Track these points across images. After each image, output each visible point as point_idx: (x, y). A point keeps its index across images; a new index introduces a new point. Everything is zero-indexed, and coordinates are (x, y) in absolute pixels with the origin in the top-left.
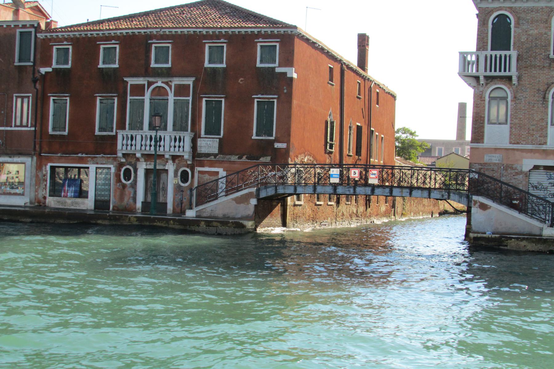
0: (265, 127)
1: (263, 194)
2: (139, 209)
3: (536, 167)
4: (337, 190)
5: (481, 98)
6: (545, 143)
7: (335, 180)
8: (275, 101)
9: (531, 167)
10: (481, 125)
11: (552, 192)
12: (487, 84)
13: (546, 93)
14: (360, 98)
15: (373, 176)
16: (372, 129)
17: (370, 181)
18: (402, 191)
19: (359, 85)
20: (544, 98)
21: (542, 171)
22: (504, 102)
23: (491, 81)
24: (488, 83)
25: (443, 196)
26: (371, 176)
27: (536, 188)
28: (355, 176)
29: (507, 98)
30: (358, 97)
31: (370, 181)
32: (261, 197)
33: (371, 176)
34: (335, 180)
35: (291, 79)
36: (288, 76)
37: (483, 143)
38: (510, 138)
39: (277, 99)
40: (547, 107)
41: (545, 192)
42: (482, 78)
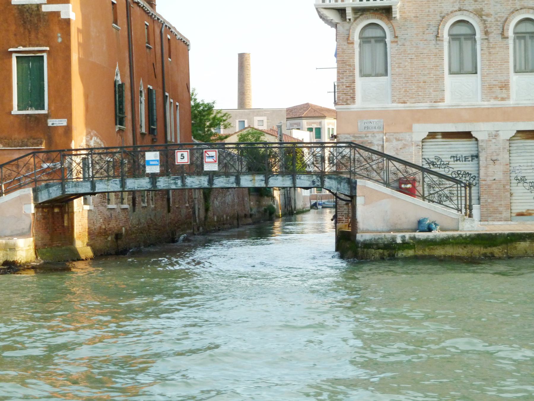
0: (33, 95)
1: (44, 197)
2: (515, 248)
3: (432, 135)
4: (158, 184)
5: (348, 39)
6: (442, 100)
7: (153, 169)
8: (45, 55)
9: (425, 135)
10: (351, 78)
11: (455, 170)
12: (356, 19)
13: (438, 29)
14: (150, 48)
15: (211, 160)
16: (167, 94)
17: (207, 168)
18: (254, 179)
19: (148, 28)
20: (502, 34)
21: (439, 140)
22: (382, 45)
23: (361, 15)
24: (358, 17)
25: (314, 182)
26: (207, 160)
27: (433, 165)
28: (183, 161)
29: (385, 37)
30: (147, 47)
31: (207, 168)
32: (40, 201)
33: (207, 160)
34: (153, 169)
35: (68, 22)
36: (63, 16)
37: (444, 102)
38: (393, 96)
39: (49, 52)
40: (441, 51)
41: (447, 169)
42: (349, 12)
